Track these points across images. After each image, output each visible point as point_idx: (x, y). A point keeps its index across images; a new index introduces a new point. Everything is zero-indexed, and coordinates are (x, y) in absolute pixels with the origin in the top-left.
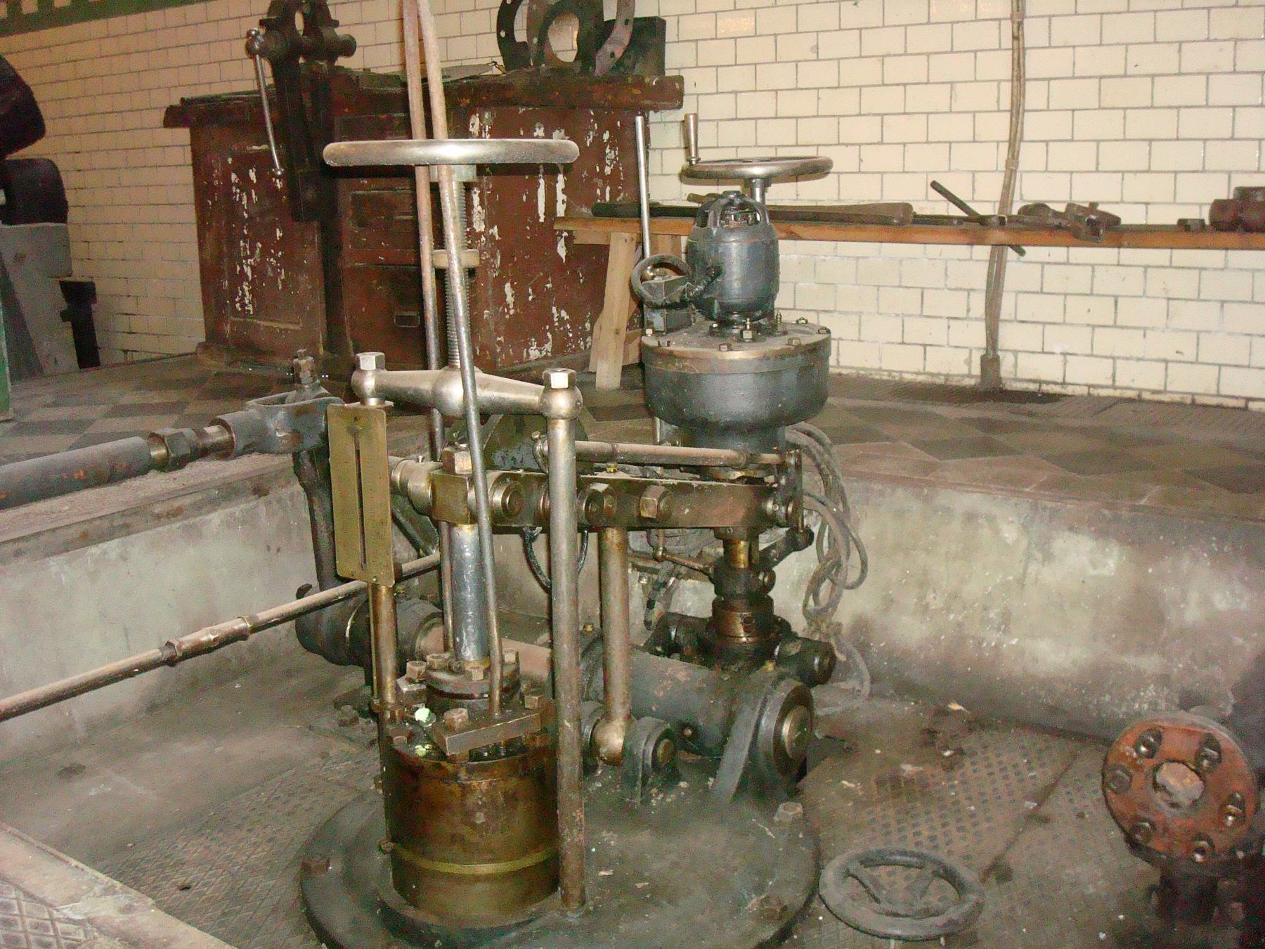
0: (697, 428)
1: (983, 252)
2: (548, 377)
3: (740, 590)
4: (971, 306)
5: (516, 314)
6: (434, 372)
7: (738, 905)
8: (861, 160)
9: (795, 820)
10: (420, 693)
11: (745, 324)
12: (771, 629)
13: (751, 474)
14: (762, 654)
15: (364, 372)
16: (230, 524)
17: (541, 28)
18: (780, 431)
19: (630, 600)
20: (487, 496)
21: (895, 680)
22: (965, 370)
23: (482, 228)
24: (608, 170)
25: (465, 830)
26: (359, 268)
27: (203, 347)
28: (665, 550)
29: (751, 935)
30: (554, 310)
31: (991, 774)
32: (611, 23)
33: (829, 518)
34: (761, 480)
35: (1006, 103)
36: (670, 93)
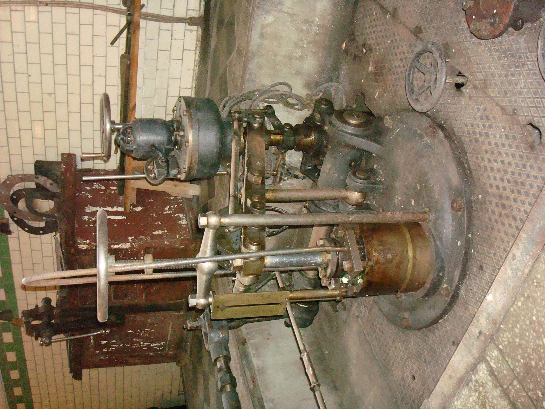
0: (223, 156)
1: (143, 23)
2: (202, 226)
3: (292, 139)
4: (167, 29)
5: (167, 230)
6: (198, 274)
7: (428, 146)
8: (100, 76)
9: (392, 119)
10: (335, 280)
11: (176, 135)
12: (309, 125)
13: (242, 133)
14: (319, 129)
15: (197, 304)
16: (258, 355)
17: (39, 216)
18: (224, 120)
19: (293, 186)
20: (253, 252)
21: (331, 72)
22: (195, 33)
24: (103, 188)
25: (394, 262)
26: (146, 297)
27: (178, 363)
28: (274, 171)
29: (442, 141)
30: (165, 213)
31: (374, 33)
32: (37, 184)
33: (262, 98)
34: (245, 128)
35: (76, 10)
36: (69, 159)
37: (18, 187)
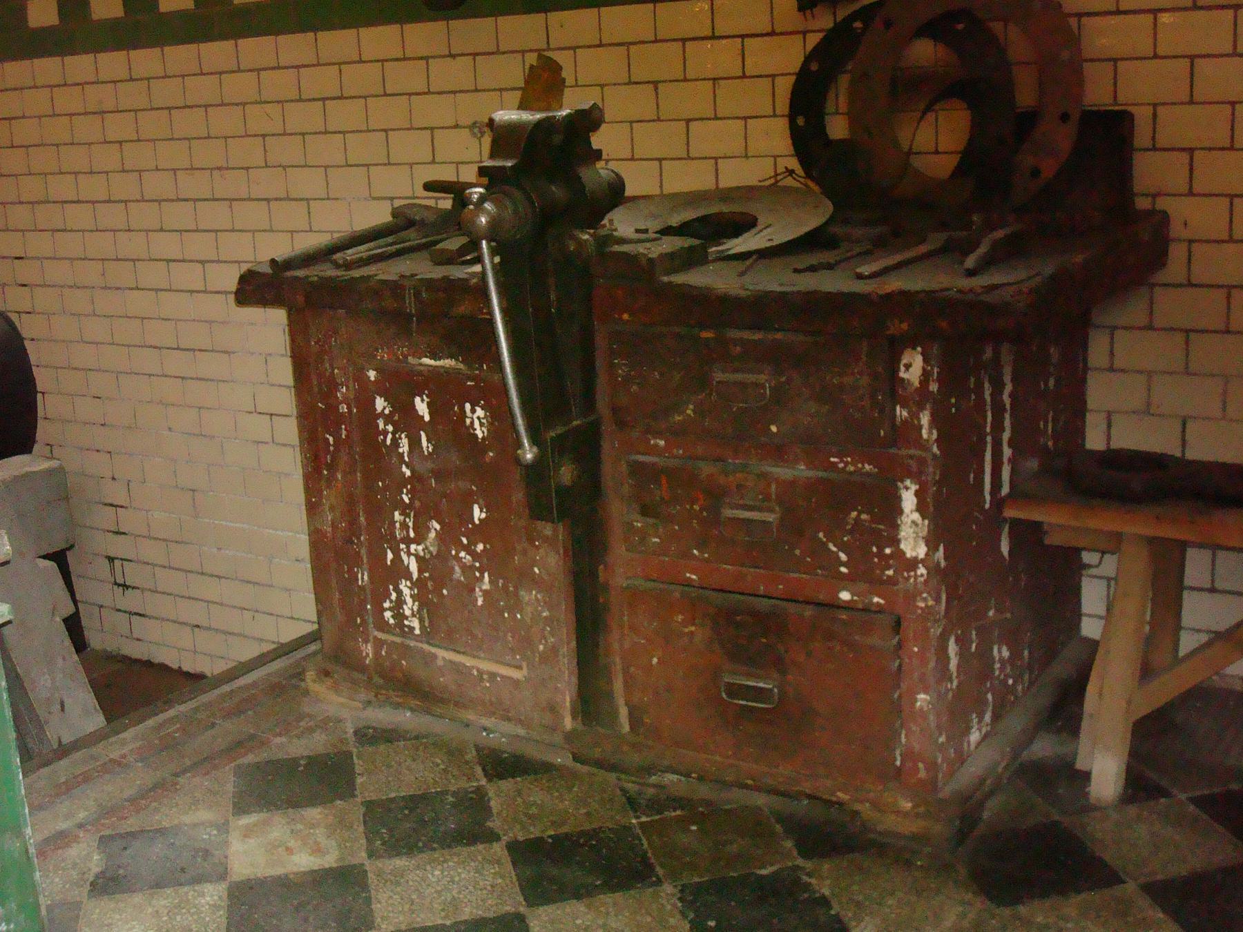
4: (458, 58)
23: (921, 551)
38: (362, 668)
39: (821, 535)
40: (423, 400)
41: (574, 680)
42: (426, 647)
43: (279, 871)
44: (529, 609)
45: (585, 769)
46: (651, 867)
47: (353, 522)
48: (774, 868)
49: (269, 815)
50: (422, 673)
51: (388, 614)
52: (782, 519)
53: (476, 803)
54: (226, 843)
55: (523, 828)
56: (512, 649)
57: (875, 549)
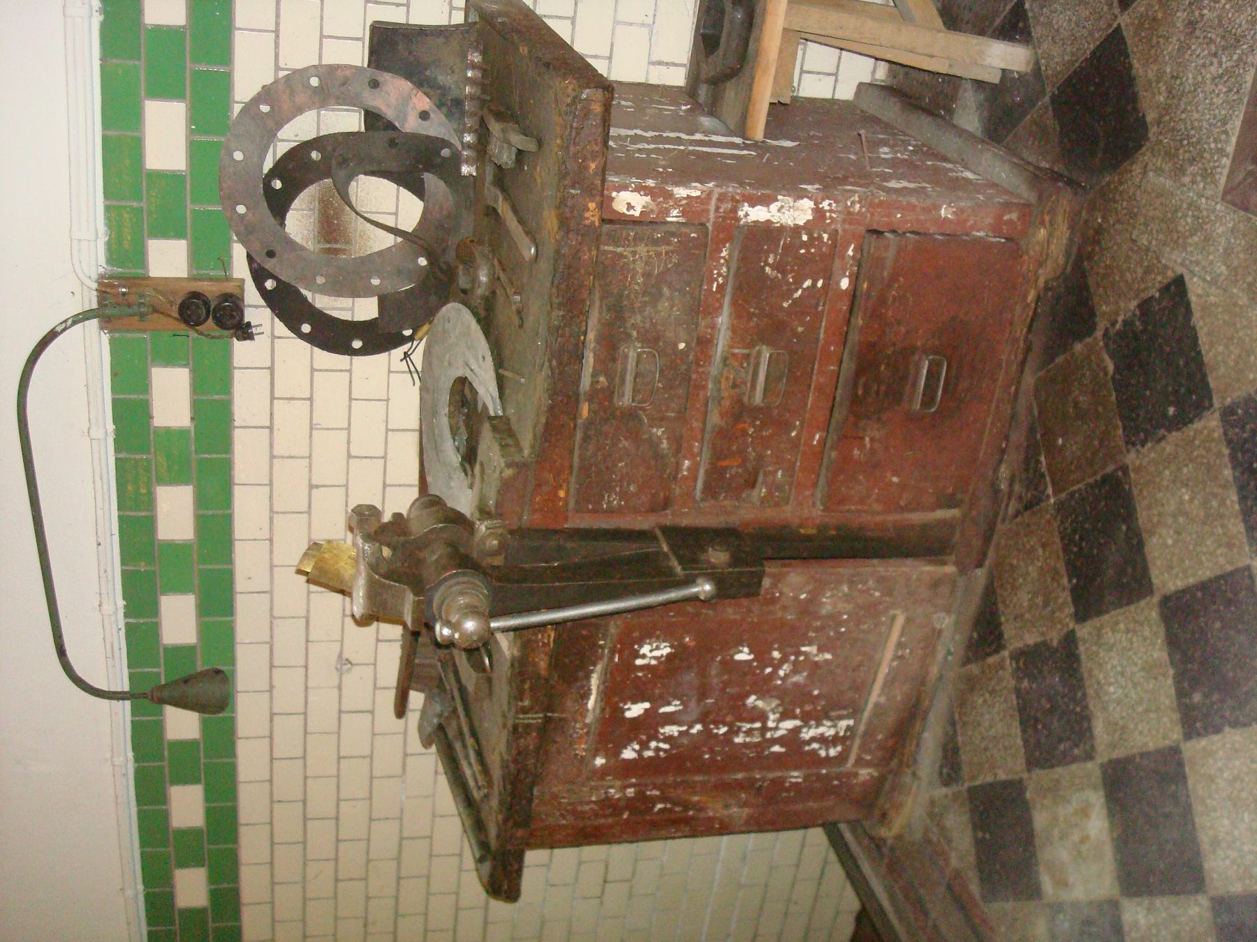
23: (807, 204)
32: (372, 118)
37: (301, 128)
38: (881, 780)
39: (785, 305)
40: (629, 709)
41: (909, 561)
42: (866, 714)
43: (1108, 849)
44: (840, 606)
45: (991, 554)
46: (1105, 479)
47: (740, 785)
48: (1106, 357)
49: (1042, 869)
50: (891, 719)
51: (833, 752)
52: (767, 345)
53: (1030, 659)
54: (1075, 905)
55: (1061, 609)
56: (876, 625)
57: (803, 251)
